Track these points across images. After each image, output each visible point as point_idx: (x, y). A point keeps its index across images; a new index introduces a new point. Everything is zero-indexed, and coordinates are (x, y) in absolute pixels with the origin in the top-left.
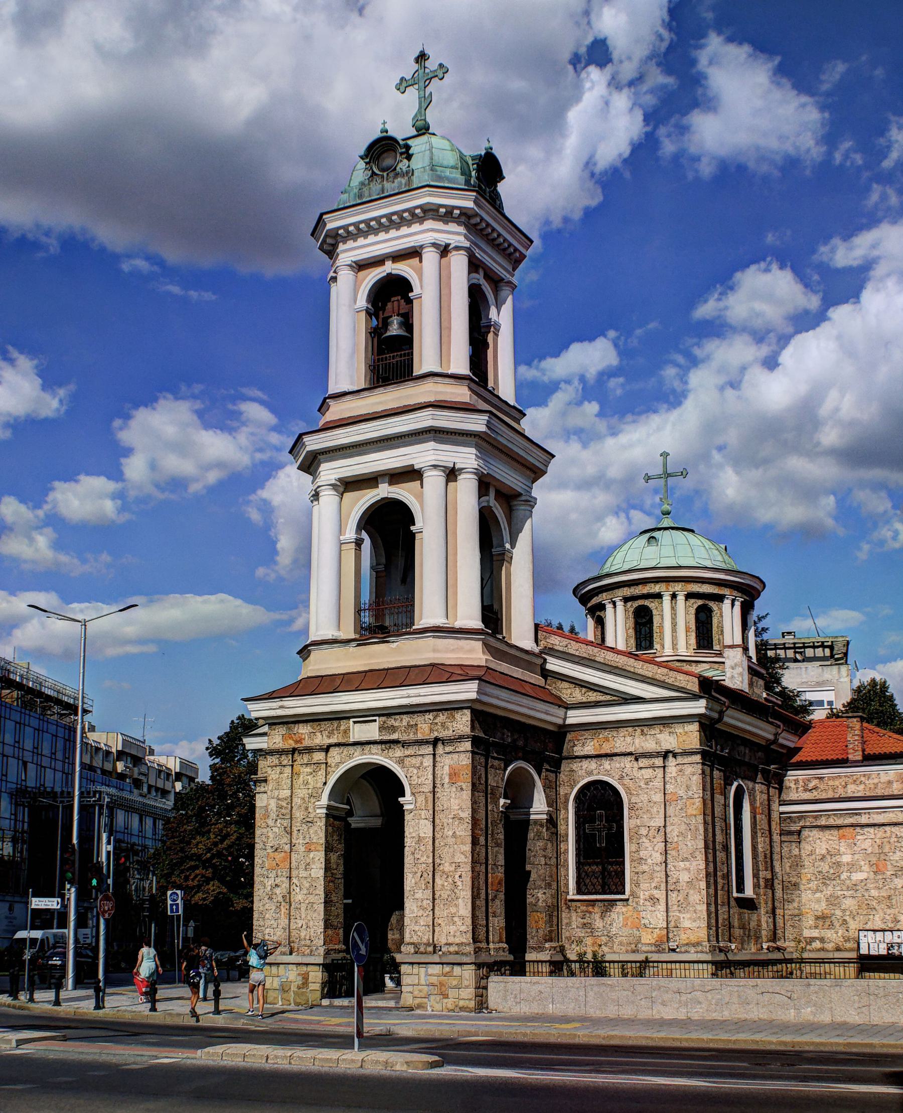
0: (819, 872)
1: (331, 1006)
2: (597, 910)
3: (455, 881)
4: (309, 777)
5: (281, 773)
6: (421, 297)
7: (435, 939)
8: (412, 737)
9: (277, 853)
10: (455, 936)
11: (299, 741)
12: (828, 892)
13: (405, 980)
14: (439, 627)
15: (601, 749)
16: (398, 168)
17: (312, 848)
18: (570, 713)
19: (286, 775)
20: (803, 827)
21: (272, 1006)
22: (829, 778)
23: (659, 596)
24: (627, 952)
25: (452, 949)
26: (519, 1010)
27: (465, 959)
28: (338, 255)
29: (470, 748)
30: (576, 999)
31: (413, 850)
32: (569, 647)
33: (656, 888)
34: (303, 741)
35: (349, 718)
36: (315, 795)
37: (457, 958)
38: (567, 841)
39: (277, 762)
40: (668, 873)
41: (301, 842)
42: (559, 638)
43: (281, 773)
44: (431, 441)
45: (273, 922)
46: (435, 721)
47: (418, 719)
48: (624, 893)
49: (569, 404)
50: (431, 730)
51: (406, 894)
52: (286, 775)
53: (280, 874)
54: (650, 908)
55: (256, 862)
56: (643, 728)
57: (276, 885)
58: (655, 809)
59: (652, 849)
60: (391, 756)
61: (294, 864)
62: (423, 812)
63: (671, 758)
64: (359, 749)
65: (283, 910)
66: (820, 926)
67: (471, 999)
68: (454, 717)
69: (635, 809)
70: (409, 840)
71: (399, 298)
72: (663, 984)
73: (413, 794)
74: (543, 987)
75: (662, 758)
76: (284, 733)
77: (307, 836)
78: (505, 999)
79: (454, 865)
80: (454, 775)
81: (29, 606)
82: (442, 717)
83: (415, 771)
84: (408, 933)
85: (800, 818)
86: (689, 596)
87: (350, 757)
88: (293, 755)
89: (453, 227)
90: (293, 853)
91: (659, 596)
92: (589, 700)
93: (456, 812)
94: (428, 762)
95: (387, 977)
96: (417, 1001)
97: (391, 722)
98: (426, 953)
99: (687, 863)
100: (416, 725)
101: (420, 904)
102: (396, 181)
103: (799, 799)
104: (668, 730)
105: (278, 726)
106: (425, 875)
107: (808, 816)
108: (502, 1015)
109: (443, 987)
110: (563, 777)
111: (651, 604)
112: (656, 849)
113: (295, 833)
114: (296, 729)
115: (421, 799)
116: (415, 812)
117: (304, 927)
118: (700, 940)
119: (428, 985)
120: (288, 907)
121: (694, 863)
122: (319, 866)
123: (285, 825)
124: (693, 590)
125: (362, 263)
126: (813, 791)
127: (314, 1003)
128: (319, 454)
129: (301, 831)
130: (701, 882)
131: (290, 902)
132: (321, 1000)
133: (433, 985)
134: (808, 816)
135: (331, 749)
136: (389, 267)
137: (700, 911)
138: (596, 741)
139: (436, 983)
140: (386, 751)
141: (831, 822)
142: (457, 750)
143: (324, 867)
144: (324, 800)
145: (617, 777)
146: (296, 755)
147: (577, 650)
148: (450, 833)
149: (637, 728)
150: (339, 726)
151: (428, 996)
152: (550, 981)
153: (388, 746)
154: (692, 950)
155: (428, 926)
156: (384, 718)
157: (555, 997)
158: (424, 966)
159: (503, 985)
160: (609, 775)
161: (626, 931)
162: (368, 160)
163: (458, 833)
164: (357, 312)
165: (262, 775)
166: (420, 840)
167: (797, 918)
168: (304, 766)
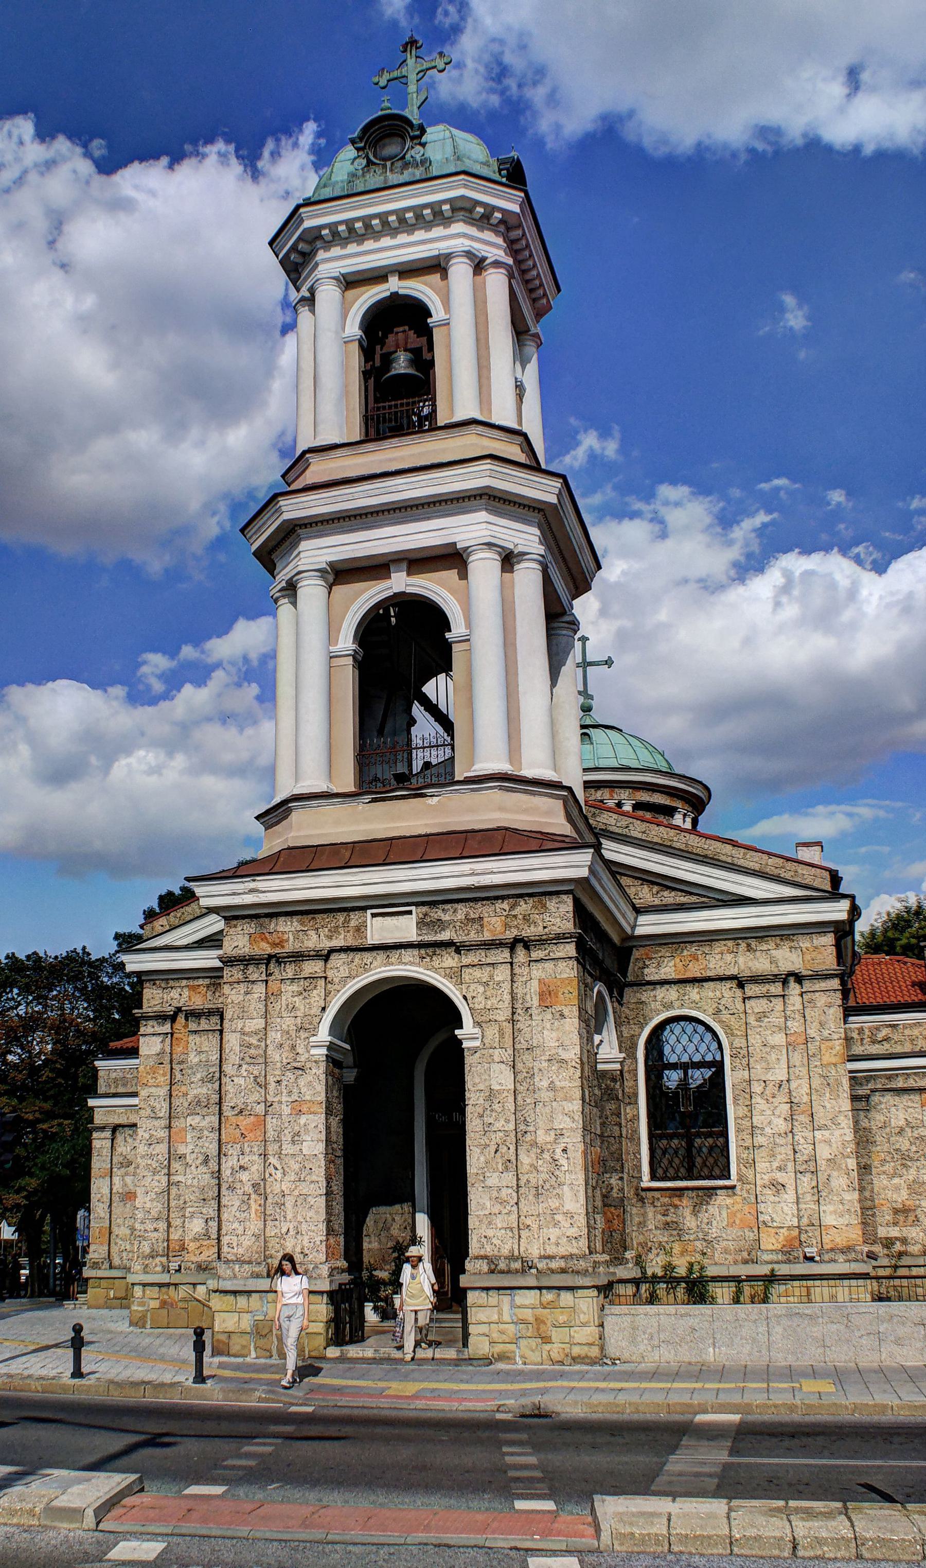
0: (897, 1150)
1: (342, 1359)
2: (686, 1202)
3: (556, 1157)
4: (296, 999)
6: (448, 324)
7: (522, 1250)
8: (473, 936)
9: (241, 1118)
10: (557, 1244)
11: (280, 944)
12: (911, 1178)
13: (474, 1315)
14: (506, 774)
15: (685, 971)
16: (408, 157)
17: (304, 1109)
18: (642, 919)
19: (256, 996)
20: (872, 1091)
21: (240, 1360)
22: (905, 1027)
24: (735, 1262)
25: (554, 1265)
26: (657, 1358)
27: (580, 1281)
28: (317, 265)
29: (573, 953)
30: (754, 1340)
31: (480, 1110)
32: (631, 827)
33: (780, 1169)
35: (364, 909)
36: (308, 1028)
37: (568, 1280)
38: (636, 1103)
39: (240, 976)
40: (796, 1148)
41: (284, 1099)
42: (615, 816)
43: (247, 993)
44: (480, 510)
45: (236, 1225)
46: (513, 913)
47: (484, 910)
48: (729, 1178)
49: (227, 685)
50: (507, 926)
51: (470, 1180)
52: (256, 996)
53: (247, 1150)
54: (772, 1198)
56: (750, 941)
57: (241, 1167)
58: (774, 1056)
59: (771, 1113)
60: (437, 966)
61: (271, 1134)
62: (497, 1052)
63: (792, 984)
64: (381, 956)
65: (254, 1207)
66: (901, 1223)
67: (590, 1344)
68: (544, 906)
69: (740, 1056)
71: (407, 328)
72: (896, 1312)
73: (478, 1024)
74: (697, 1321)
75: (780, 984)
76: (252, 931)
78: (633, 1341)
79: (552, 1133)
80: (547, 996)
82: (524, 907)
83: (481, 989)
84: (475, 1240)
85: (868, 1079)
87: (366, 968)
88: (267, 965)
89: (488, 235)
90: (269, 1118)
92: (664, 903)
93: (553, 1052)
94: (502, 973)
95: (368, 1308)
96: (498, 1348)
97: (438, 913)
98: (509, 1272)
99: (826, 1133)
100: (481, 918)
101: (495, 1194)
102: (405, 172)
103: (866, 1053)
104: (788, 944)
105: (240, 922)
106: (503, 1149)
107: (880, 1077)
108: (626, 1367)
109: (542, 1326)
110: (627, 1011)
112: (777, 1112)
113: (272, 1087)
114: (272, 925)
115: (492, 1032)
117: (292, 1232)
118: (850, 1243)
119: (516, 1323)
120: (262, 1202)
121: (837, 1133)
122: (316, 1136)
123: (256, 1073)
124: (643, 799)
125: (350, 279)
126: (884, 1043)
127: (313, 1354)
128: (300, 526)
129: (284, 1083)
130: (848, 1160)
131: (265, 1193)
132: (325, 1348)
133: (524, 1322)
134: (880, 1077)
135: (334, 957)
136: (394, 284)
137: (850, 1201)
138: (678, 960)
139: (531, 1319)
140: (428, 959)
141: (911, 1083)
142: (552, 955)
143: (324, 1138)
144: (324, 1034)
145: (711, 1011)
146: (272, 965)
147: (644, 832)
148: (545, 1084)
149: (740, 941)
150: (347, 921)
151: (515, 1341)
152: (709, 1312)
153: (430, 951)
154: (841, 1258)
155: (511, 1229)
156: (424, 909)
157: (718, 1336)
158: (509, 1292)
159: (628, 1319)
160: (698, 1009)
161: (734, 1232)
162: (362, 145)
163: (558, 1083)
164: (345, 342)
165: (150, 1010)
166: (491, 1095)
167: (870, 1213)
168: (288, 982)
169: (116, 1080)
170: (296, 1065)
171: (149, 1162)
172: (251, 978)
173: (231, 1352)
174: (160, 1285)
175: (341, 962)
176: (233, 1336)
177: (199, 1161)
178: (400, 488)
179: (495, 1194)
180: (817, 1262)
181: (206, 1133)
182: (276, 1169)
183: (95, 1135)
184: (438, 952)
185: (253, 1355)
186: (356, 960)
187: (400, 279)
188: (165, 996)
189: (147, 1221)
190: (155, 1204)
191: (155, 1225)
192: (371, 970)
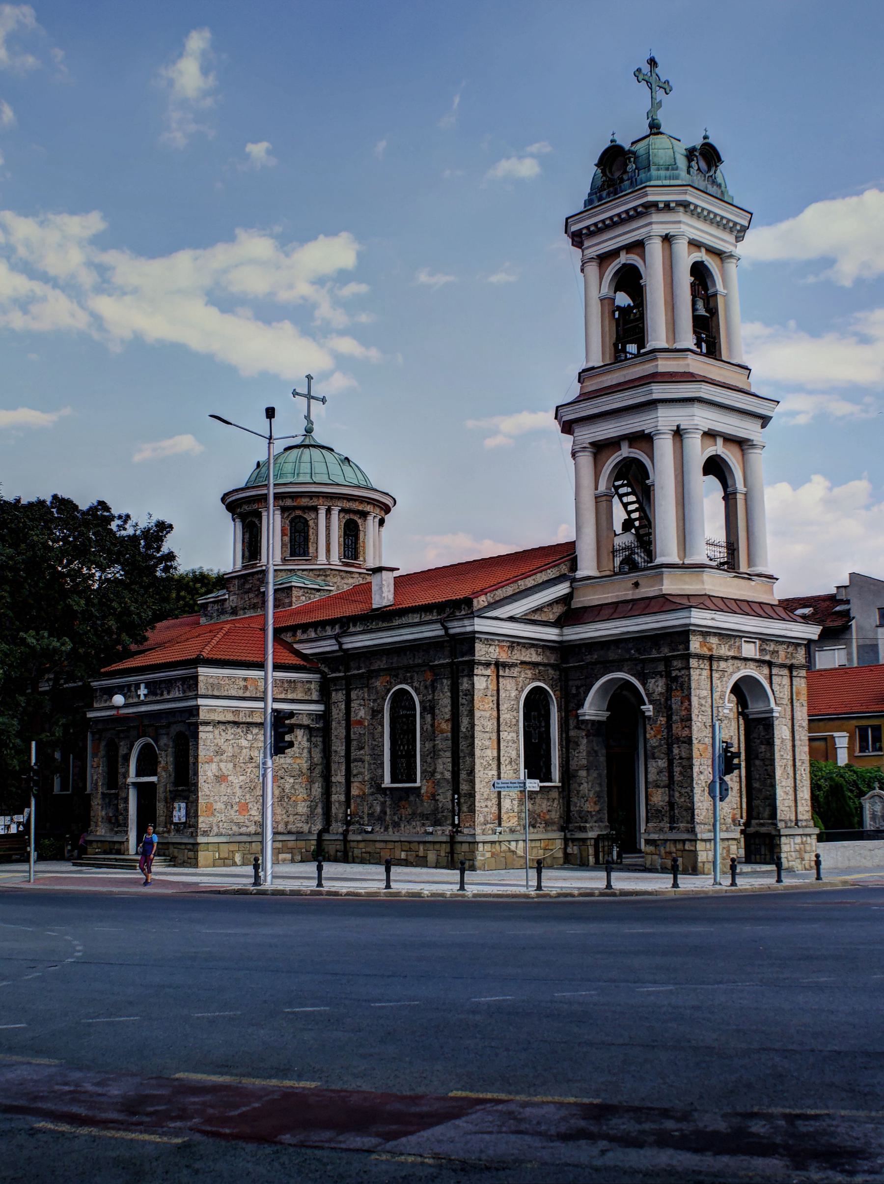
43: (700, 675)
55: (476, 745)
81: (211, 416)
87: (738, 669)
91: (315, 509)
111: (310, 516)
166: (783, 741)
169: (212, 685)
171: (482, 761)
176: (706, 864)
177: (507, 762)
178: (673, 391)
181: (510, 744)
183: (201, 728)
187: (627, 253)
190: (486, 789)
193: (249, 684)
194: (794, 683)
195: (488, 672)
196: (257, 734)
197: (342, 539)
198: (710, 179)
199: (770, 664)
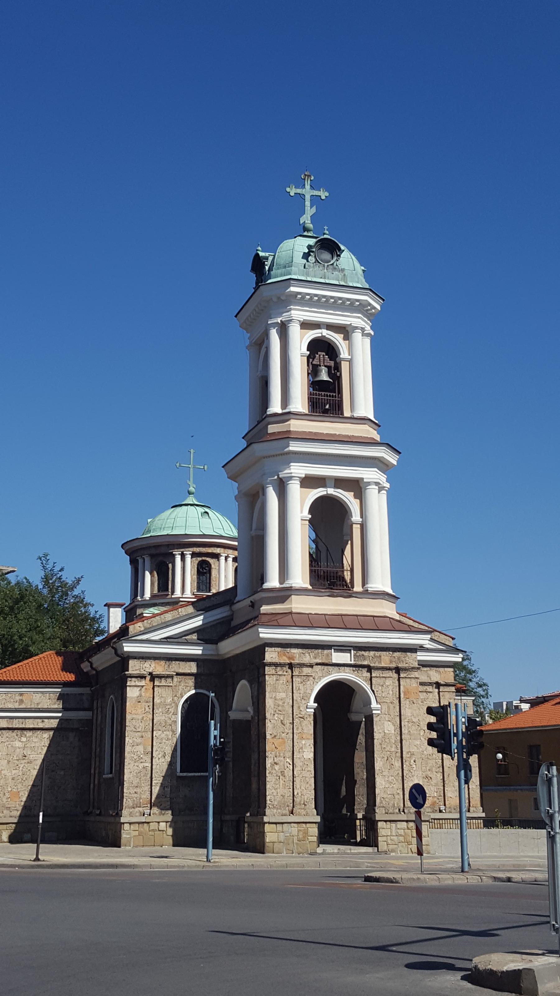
3: (411, 764)
4: (300, 685)
5: (277, 680)
8: (377, 665)
9: (275, 739)
19: (281, 682)
23: (217, 556)
34: (295, 659)
39: (274, 672)
43: (277, 680)
45: (273, 791)
51: (377, 772)
62: (387, 716)
70: (377, 734)
77: (300, 728)
83: (380, 688)
86: (194, 555)
93: (410, 718)
96: (391, 847)
98: (394, 813)
101: (386, 779)
106: (390, 759)
116: (381, 716)
142: (409, 676)
170: (301, 716)
171: (132, 755)
172: (279, 673)
173: (275, 851)
174: (139, 823)
175: (319, 669)
177: (160, 756)
179: (386, 779)
180: (444, 813)
181: (164, 741)
182: (290, 764)
184: (361, 669)
185: (285, 852)
186: (325, 669)
188: (141, 665)
189: (131, 788)
191: (135, 790)
192: (332, 674)
193: (24, 698)
194: (401, 683)
195: (143, 683)
196: (30, 737)
197: (195, 577)
198: (331, 267)
199: (370, 669)
